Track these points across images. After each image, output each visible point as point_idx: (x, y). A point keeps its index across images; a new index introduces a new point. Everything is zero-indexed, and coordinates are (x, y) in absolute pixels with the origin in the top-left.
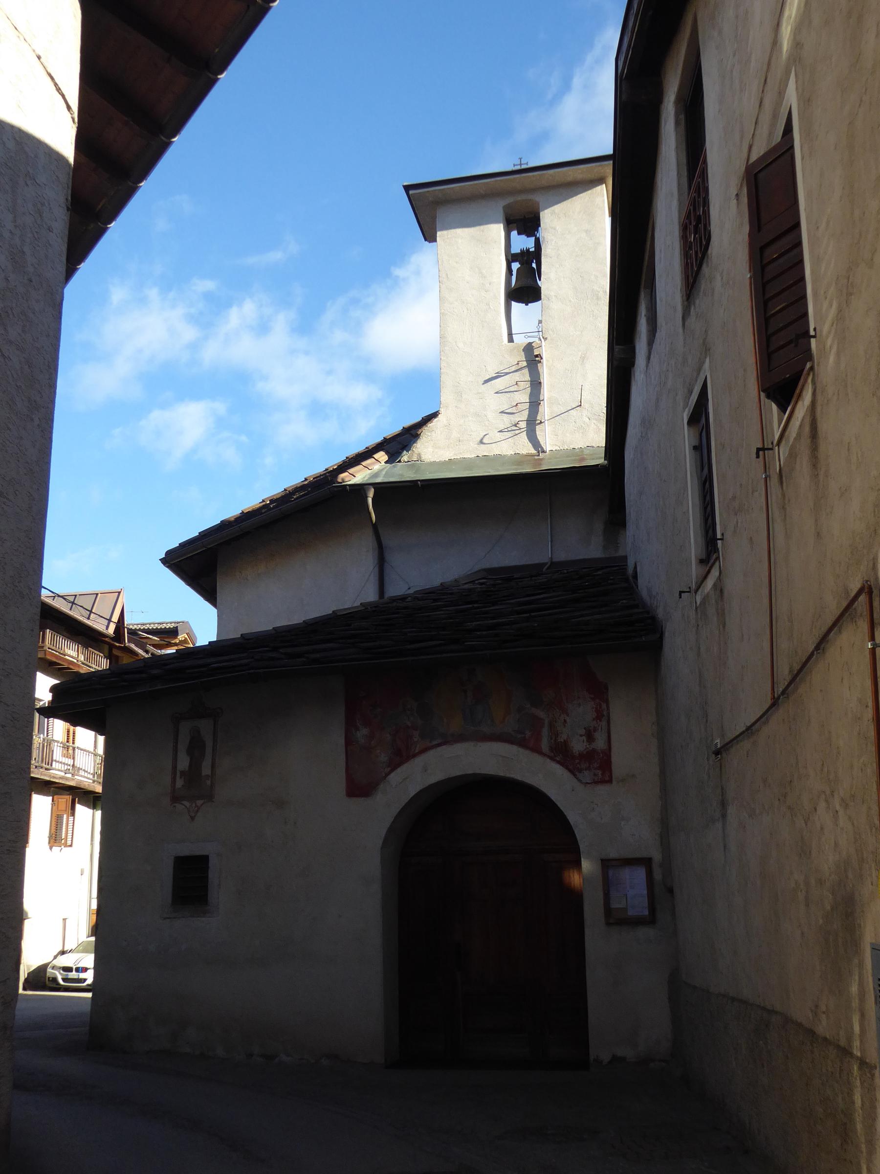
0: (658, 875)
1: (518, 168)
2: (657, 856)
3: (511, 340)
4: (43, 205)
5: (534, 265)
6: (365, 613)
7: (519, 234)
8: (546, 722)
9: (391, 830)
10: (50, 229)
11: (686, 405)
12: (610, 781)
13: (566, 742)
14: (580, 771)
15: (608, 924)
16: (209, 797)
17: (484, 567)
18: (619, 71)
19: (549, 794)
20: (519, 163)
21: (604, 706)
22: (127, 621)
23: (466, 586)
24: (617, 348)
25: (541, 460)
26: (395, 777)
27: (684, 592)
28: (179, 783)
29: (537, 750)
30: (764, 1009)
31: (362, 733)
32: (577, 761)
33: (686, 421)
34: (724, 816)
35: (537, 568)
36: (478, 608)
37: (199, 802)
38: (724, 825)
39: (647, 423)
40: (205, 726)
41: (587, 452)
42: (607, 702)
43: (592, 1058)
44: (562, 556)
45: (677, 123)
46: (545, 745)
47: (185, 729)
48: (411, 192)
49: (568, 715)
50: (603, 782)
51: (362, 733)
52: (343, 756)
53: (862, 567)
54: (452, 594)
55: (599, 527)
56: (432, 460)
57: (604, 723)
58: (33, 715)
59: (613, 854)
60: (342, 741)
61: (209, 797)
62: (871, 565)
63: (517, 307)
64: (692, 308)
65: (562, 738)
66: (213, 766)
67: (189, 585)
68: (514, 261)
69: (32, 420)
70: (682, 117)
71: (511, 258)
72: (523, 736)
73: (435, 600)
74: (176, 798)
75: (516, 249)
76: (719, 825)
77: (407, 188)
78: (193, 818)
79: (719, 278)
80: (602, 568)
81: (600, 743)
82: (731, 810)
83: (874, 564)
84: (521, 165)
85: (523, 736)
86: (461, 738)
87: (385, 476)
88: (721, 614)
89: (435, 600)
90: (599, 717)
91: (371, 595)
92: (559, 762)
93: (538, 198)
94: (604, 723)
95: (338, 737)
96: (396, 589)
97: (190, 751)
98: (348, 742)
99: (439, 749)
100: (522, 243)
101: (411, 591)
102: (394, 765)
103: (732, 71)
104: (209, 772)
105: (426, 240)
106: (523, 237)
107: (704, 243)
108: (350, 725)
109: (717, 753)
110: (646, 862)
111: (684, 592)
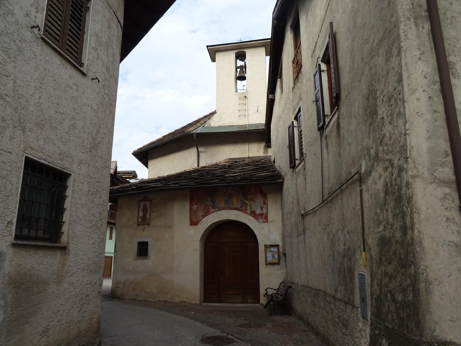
0: (281, 250)
1: (239, 42)
2: (281, 244)
3: (236, 91)
4: (114, 54)
5: (244, 70)
6: (195, 171)
7: (240, 60)
8: (249, 204)
9: (203, 235)
10: (116, 61)
11: (293, 114)
12: (267, 222)
13: (255, 211)
14: (259, 219)
15: (266, 264)
16: (149, 225)
17: (228, 158)
18: (274, 17)
19: (250, 226)
21: (266, 200)
22: (119, 170)
23: (224, 164)
25: (246, 127)
26: (204, 220)
28: (140, 220)
29: (247, 213)
30: (317, 290)
32: (258, 216)
34: (304, 234)
35: (243, 159)
36: (228, 170)
37: (146, 226)
38: (304, 236)
39: (279, 118)
40: (148, 204)
41: (259, 125)
44: (251, 155)
46: (248, 211)
47: (142, 204)
48: (208, 48)
49: (255, 203)
50: (265, 222)
51: (195, 207)
53: (356, 166)
54: (219, 166)
56: (214, 126)
57: (266, 205)
59: (268, 243)
60: (189, 209)
61: (149, 225)
62: (359, 166)
63: (238, 82)
64: (296, 86)
65: (253, 210)
66: (150, 216)
67: (140, 161)
68: (238, 68)
69: (110, 116)
71: (237, 68)
73: (215, 168)
74: (139, 225)
75: (238, 65)
76: (303, 236)
77: (207, 46)
78: (144, 231)
79: (305, 79)
80: (263, 159)
81: (265, 211)
82: (307, 232)
83: (360, 166)
84: (240, 41)
86: (224, 209)
87: (200, 130)
88: (305, 175)
89: (215, 168)
90: (265, 203)
91: (195, 166)
92: (252, 216)
94: (266, 205)
95: (187, 207)
96: (202, 164)
97: (143, 211)
98: (191, 209)
100: (240, 63)
101: (207, 165)
102: (204, 216)
103: (310, 20)
104: (149, 217)
105: (212, 61)
107: (300, 68)
108: (191, 204)
109: (302, 215)
110: (277, 246)
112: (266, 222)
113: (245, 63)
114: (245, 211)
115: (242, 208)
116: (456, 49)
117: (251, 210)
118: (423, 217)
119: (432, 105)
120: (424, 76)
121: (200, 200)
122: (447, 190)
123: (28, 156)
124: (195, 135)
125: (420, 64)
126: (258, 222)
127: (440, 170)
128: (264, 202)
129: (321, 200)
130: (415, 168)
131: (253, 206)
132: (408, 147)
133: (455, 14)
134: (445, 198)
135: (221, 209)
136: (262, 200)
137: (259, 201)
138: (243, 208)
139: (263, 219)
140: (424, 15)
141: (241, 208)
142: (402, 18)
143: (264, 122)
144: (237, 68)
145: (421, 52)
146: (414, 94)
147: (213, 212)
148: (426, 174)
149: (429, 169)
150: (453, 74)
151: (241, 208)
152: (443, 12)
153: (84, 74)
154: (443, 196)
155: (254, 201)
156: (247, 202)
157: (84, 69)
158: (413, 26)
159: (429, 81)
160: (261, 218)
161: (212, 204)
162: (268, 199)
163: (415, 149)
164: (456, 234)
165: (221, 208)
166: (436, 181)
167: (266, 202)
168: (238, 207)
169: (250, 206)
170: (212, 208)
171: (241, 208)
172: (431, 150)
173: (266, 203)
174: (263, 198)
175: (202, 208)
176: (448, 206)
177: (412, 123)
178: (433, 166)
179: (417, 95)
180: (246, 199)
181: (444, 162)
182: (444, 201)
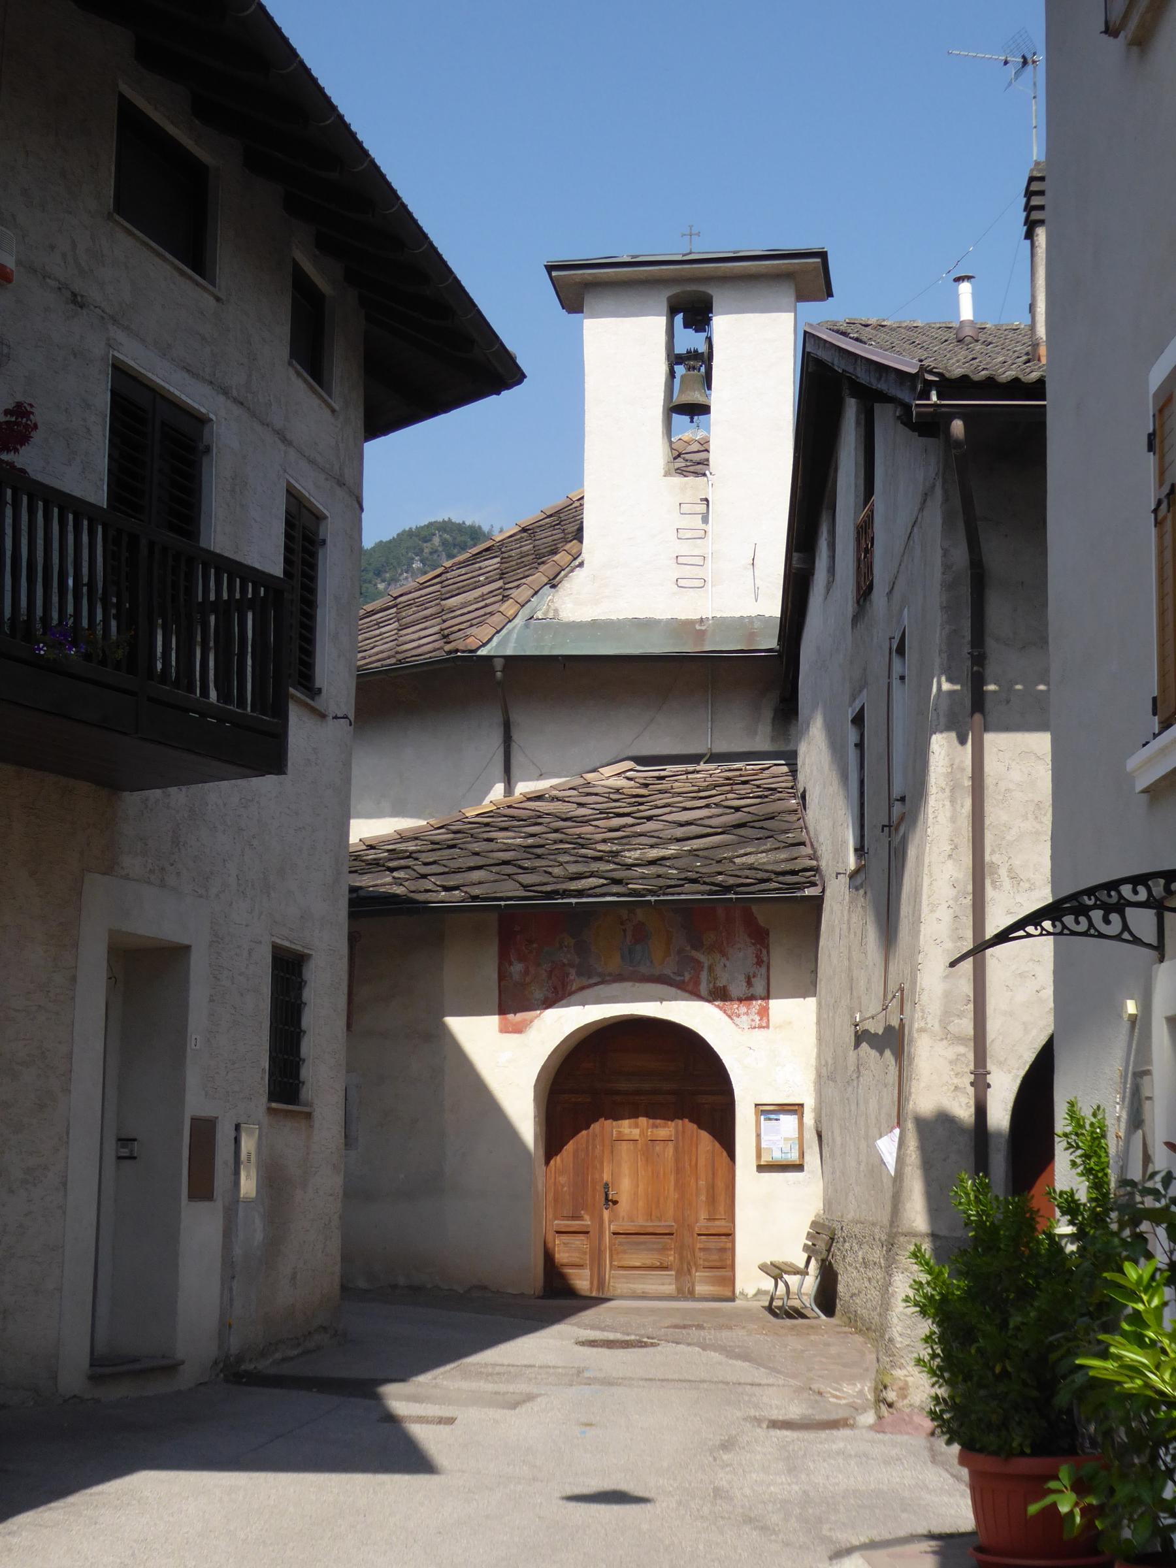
2: (809, 1102)
8: (706, 965)
12: (767, 1027)
14: (738, 1016)
20: (688, 233)
21: (764, 952)
24: (796, 555)
27: (840, 874)
31: (517, 968)
33: (850, 719)
41: (757, 625)
42: (767, 947)
43: (737, 1292)
45: (858, 423)
46: (704, 992)
48: (554, 274)
49: (728, 959)
50: (760, 1027)
51: (517, 968)
52: (497, 992)
55: (768, 714)
57: (763, 970)
58: (1054, 1210)
60: (496, 976)
65: (720, 984)
68: (677, 364)
70: (863, 416)
72: (682, 978)
75: (680, 349)
77: (550, 268)
85: (682, 978)
90: (759, 962)
93: (714, 291)
94: (763, 970)
98: (502, 976)
99: (597, 988)
100: (689, 340)
106: (690, 331)
108: (504, 957)
110: (795, 1109)
111: (840, 874)
112: (764, 1027)
113: (709, 340)
114: (690, 988)
115: (683, 976)
116: (1004, 843)
117: (711, 986)
118: (922, 1085)
119: (957, 929)
120: (951, 883)
121: (535, 945)
122: (962, 1049)
123: (279, 941)
124: (499, 664)
125: (950, 863)
126: (737, 1025)
127: (956, 1021)
128: (758, 957)
129: (969, 934)
130: (923, 1018)
131: (718, 969)
132: (918, 990)
133: (1012, 786)
134: (957, 1059)
135: (608, 978)
136: (750, 952)
137: (741, 955)
138: (687, 977)
139: (751, 1017)
140: (966, 785)
141: (680, 975)
142: (934, 787)
143: (771, 606)
144: (673, 358)
145: (953, 847)
146: (935, 911)
147: (582, 988)
148: (937, 1027)
149: (940, 1021)
150: (993, 882)
151: (678, 978)
152: (994, 782)
153: (323, 716)
154: (955, 1057)
155: (724, 954)
156: (702, 958)
157: (318, 704)
158: (947, 803)
159: (958, 892)
160: (747, 1014)
161: (577, 960)
162: (771, 951)
163: (925, 992)
164: (964, 1107)
165: (610, 974)
166: (949, 1036)
167: (765, 959)
168: (668, 971)
169: (711, 969)
170: (579, 974)
171: (678, 978)
172: (947, 995)
173: (765, 964)
174: (754, 944)
175: (544, 975)
176: (960, 1070)
177: (926, 954)
178: (946, 1017)
179: (937, 914)
180: (697, 944)
181: (964, 1011)
182: (956, 1064)
